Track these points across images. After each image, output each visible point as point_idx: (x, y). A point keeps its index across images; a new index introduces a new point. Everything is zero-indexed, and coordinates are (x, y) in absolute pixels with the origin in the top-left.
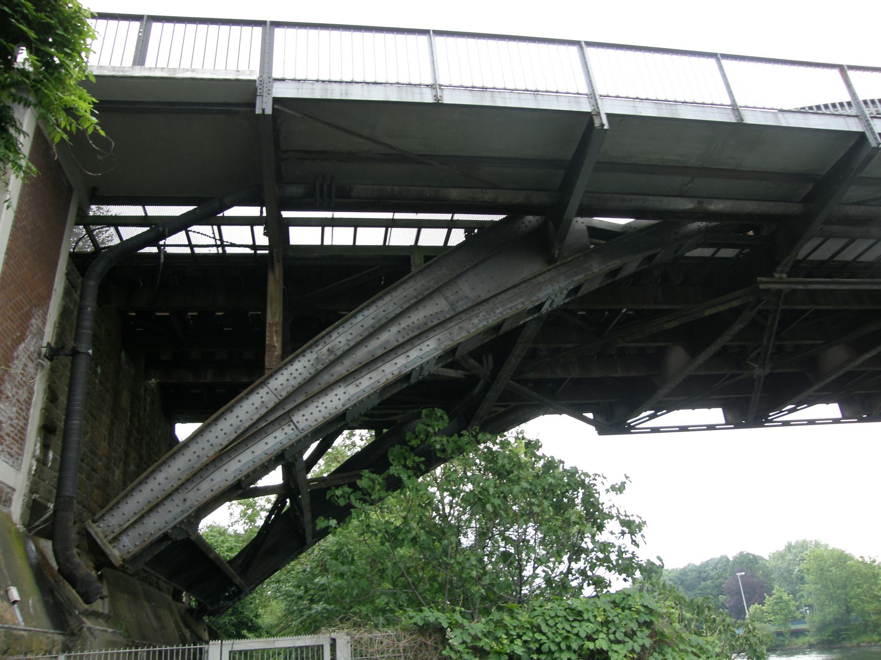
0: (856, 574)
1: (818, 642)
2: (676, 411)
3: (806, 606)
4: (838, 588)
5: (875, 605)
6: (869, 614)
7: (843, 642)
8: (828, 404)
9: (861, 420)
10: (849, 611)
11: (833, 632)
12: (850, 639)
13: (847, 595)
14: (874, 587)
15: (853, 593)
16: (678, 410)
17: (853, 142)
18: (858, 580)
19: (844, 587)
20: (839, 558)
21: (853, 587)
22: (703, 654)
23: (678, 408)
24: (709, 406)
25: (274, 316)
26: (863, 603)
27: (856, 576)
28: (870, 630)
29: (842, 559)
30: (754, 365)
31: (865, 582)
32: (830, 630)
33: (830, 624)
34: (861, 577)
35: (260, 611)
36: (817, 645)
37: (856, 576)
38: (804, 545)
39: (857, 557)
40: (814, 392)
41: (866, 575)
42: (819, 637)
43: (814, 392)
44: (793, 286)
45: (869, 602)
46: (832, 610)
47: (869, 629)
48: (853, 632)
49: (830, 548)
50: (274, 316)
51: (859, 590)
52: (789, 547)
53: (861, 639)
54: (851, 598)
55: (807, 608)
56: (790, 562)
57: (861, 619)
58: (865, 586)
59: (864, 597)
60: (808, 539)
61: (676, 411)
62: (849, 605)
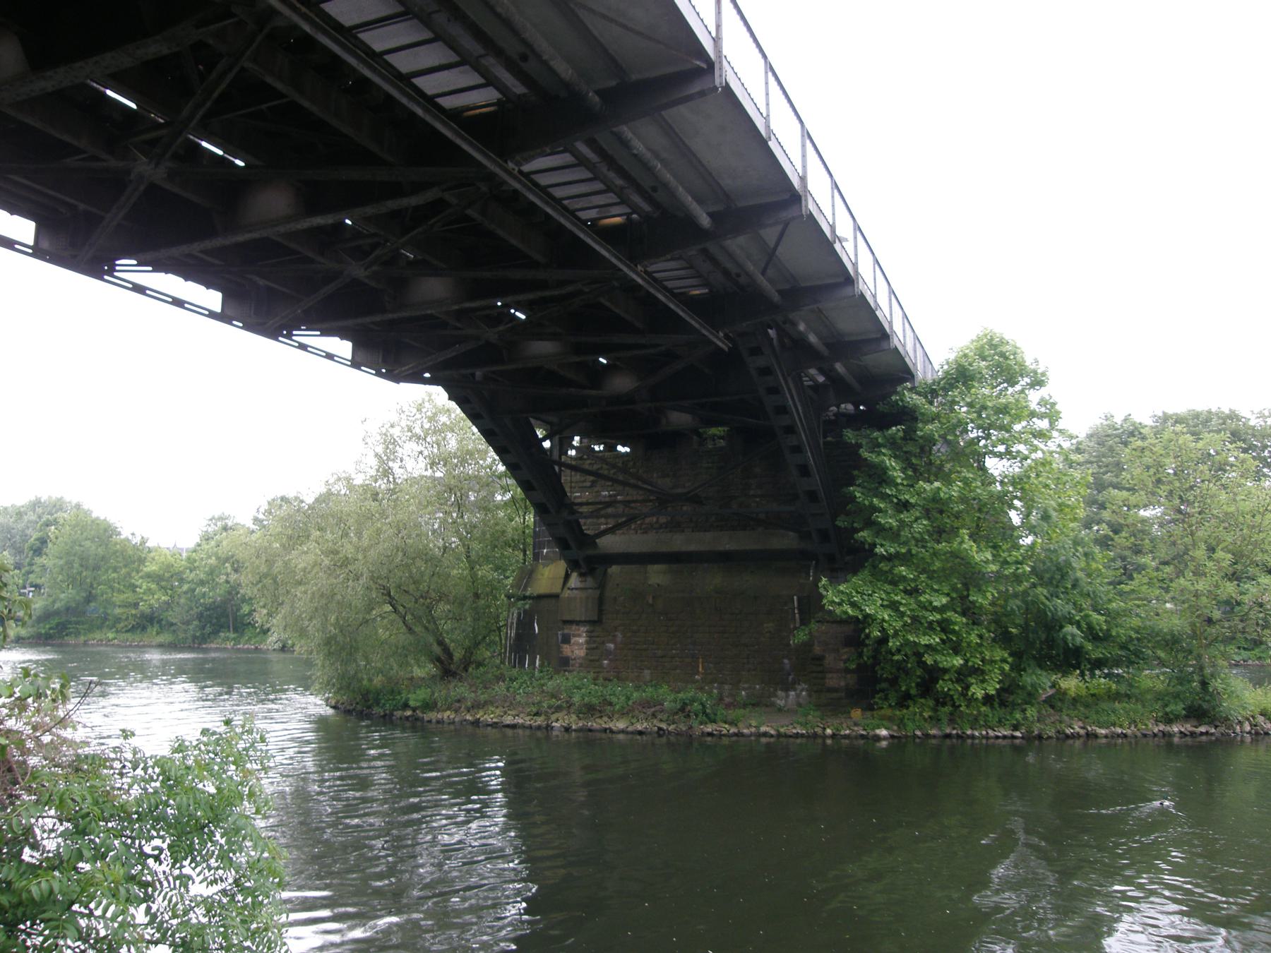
0: (118, 554)
1: (32, 636)
2: (163, 274)
3: (31, 587)
4: (87, 569)
5: (126, 595)
6: (115, 606)
7: (66, 638)
8: (208, 288)
9: (379, 374)
10: (90, 598)
11: (58, 625)
12: (78, 634)
13: (95, 578)
14: (134, 574)
15: (105, 577)
16: (342, 338)
17: (786, 196)
18: (118, 562)
19: (96, 568)
20: (106, 530)
21: (107, 571)
22: (242, 608)
23: (192, 281)
24: (208, 285)
25: (154, 48)
26: (113, 591)
27: (117, 557)
28: (108, 626)
29: (105, 533)
30: (139, 155)
31: (125, 566)
32: (54, 621)
33: (57, 613)
34: (124, 559)
35: (1135, 576)
36: (29, 638)
37: (117, 557)
38: (58, 505)
39: (125, 534)
40: (201, 252)
41: (130, 557)
42: (35, 629)
43: (201, 252)
44: (296, 19)
45: (119, 591)
46: (67, 596)
47: (107, 623)
48: (85, 626)
49: (94, 515)
50: (154, 48)
51: (115, 575)
52: (36, 504)
53: (91, 636)
54: (99, 584)
55: (33, 589)
56: (29, 525)
57: (102, 610)
58: (124, 571)
59: (116, 585)
60: (67, 499)
61: (163, 274)
62: (94, 591)
